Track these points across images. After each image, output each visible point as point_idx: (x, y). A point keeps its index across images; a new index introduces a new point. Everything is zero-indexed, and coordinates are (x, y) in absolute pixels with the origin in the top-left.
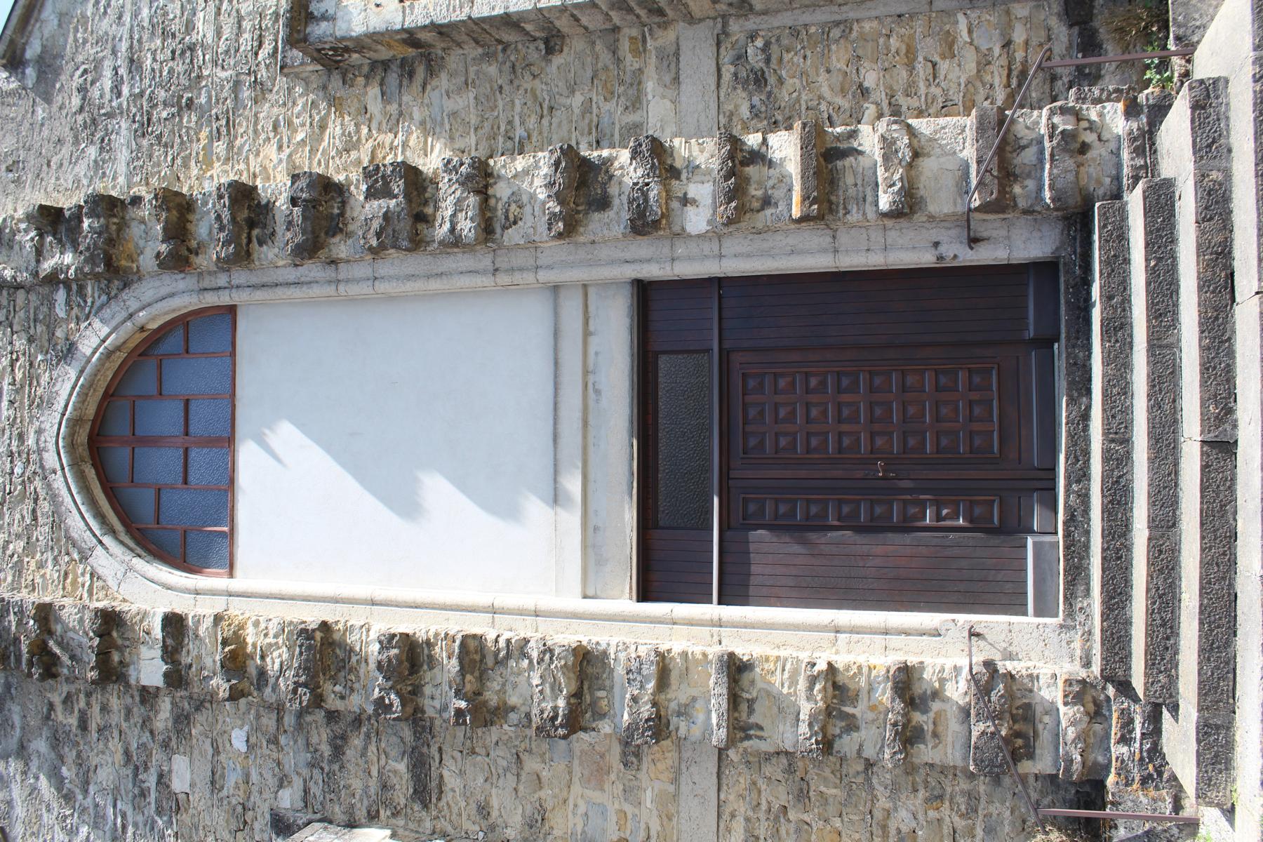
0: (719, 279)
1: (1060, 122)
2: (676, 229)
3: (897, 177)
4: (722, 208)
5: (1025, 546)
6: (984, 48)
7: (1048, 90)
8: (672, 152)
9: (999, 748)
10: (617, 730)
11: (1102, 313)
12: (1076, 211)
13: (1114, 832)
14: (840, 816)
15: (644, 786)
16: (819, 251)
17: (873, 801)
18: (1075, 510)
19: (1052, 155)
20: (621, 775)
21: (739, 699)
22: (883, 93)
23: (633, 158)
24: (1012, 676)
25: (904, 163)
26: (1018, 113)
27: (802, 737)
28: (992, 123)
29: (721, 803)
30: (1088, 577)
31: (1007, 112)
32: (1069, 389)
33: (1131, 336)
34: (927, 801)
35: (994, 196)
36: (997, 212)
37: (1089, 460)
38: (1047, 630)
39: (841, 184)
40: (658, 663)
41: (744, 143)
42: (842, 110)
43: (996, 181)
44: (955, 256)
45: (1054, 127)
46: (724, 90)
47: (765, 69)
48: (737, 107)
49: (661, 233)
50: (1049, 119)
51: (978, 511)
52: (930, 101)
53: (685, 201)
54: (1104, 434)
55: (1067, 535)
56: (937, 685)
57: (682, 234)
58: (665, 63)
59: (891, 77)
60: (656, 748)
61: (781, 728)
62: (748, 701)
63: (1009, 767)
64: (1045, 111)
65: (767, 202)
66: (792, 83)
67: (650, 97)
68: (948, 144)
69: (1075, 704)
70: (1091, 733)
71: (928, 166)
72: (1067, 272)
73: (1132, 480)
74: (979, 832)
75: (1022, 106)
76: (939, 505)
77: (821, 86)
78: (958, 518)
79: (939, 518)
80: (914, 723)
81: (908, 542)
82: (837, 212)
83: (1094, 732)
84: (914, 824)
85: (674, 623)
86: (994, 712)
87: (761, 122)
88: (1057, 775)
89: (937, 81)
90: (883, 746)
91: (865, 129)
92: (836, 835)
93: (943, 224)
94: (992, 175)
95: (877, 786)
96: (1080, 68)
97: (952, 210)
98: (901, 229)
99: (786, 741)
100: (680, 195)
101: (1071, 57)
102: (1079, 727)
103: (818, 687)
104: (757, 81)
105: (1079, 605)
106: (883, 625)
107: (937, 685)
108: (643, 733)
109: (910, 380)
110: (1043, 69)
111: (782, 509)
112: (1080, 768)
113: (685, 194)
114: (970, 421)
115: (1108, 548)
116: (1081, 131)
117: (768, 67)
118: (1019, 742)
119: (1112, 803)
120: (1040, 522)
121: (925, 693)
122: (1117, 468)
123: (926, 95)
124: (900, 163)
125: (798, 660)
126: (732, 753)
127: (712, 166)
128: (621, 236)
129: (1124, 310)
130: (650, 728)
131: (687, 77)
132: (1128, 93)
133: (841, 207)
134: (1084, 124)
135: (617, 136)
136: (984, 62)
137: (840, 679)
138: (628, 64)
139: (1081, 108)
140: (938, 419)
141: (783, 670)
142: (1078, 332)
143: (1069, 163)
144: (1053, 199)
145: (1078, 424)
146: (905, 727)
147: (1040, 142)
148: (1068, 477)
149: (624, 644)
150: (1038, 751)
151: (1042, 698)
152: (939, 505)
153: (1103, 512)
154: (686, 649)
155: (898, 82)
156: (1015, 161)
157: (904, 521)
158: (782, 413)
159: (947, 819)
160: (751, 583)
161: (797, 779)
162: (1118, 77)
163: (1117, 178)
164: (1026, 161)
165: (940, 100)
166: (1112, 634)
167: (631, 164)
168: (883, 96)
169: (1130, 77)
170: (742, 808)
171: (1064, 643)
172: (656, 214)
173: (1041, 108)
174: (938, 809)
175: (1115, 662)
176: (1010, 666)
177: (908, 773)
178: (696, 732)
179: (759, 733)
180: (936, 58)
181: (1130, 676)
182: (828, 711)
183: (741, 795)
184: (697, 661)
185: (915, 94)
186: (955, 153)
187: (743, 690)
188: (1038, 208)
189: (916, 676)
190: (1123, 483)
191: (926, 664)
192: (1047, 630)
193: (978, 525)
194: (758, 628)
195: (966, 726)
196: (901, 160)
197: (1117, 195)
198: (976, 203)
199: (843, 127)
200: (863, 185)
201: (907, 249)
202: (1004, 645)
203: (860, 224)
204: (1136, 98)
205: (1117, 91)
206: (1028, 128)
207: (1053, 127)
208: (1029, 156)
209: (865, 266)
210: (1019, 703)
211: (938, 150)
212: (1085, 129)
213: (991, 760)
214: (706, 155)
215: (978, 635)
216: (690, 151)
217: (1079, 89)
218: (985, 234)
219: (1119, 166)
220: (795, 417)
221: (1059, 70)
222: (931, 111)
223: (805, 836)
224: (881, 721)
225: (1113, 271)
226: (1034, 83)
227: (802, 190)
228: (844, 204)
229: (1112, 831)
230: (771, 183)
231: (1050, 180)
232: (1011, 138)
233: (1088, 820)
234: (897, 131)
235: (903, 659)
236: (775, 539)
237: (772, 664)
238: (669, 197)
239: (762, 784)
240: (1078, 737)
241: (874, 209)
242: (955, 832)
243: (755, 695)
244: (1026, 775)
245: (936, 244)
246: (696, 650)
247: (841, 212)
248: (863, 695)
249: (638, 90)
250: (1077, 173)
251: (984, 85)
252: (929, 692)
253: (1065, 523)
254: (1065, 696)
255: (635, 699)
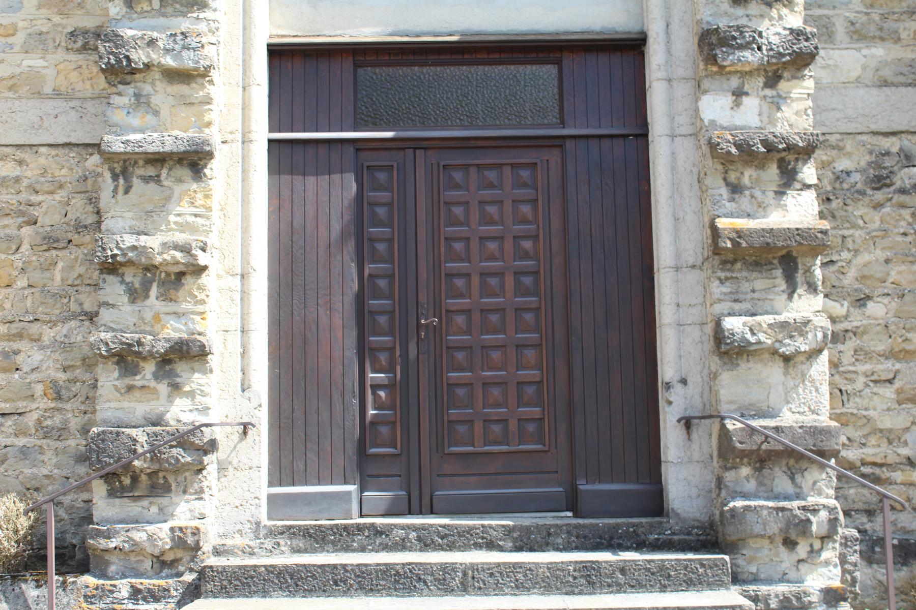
0: (645, 135)
1: (818, 523)
2: (706, 84)
3: (762, 337)
4: (730, 138)
5: (345, 483)
6: (908, 437)
7: (856, 507)
8: (797, 78)
9: (120, 459)
10: (114, 22)
11: (606, 562)
12: (720, 535)
13: (33, 584)
14: (30, 286)
15: (49, 57)
16: (677, 250)
17: (49, 322)
18: (387, 536)
19: (783, 509)
20: (60, 29)
21: (159, 164)
22: (859, 324)
23: (792, 31)
24: (200, 471)
25: (777, 345)
26: (833, 473)
27: (119, 239)
28: (820, 444)
29: (35, 149)
30: (314, 551)
31: (833, 460)
32: (521, 528)
33: (581, 593)
34: (54, 382)
35: (738, 445)
36: (720, 449)
37: (443, 550)
38: (253, 508)
39: (755, 274)
40: (196, 69)
41: (805, 162)
42: (841, 276)
43: (755, 447)
44: (670, 403)
45: (815, 511)
46: (870, 140)
47: (892, 188)
48: (849, 155)
49: (702, 66)
50: (824, 506)
51: (384, 430)
52: (849, 376)
53: (739, 94)
54: (472, 565)
55: (360, 528)
56: (187, 388)
57: (699, 89)
58: (905, 70)
59: (878, 333)
60: (95, 70)
61: (129, 215)
62: (158, 176)
63: (98, 470)
64: (833, 502)
65: (736, 189)
66: (875, 219)
67: (865, 52)
68: (798, 395)
69: (173, 539)
70: (141, 558)
71: (774, 372)
72: (651, 525)
73: (421, 595)
74: (22, 441)
75: (839, 478)
76: (389, 387)
77: (870, 252)
78: (375, 409)
79: (375, 387)
80: (142, 364)
81: (347, 353)
82: (722, 270)
83: (142, 561)
84: (26, 369)
85: (244, 88)
86: (160, 452)
87: (830, 183)
88: (92, 522)
89: (871, 384)
90: (113, 330)
91: (818, 301)
92: (6, 282)
93: (707, 389)
94: (762, 443)
95: (67, 326)
96: (881, 541)
97: (723, 398)
98: (702, 342)
99: (113, 221)
100: (746, 88)
101: (893, 532)
102: (146, 544)
103: (179, 255)
104: (879, 178)
105: (282, 542)
106: (252, 327)
107: (187, 388)
108: (112, 53)
109: (530, 354)
110: (881, 501)
111: (381, 211)
112: (101, 547)
113: (747, 94)
114: (485, 421)
115: (347, 571)
116: (810, 541)
117: (895, 192)
118: (127, 481)
119: (64, 582)
120: (371, 498)
121: (178, 376)
122: (435, 580)
123: (855, 372)
124: (777, 341)
125: (208, 232)
126: (95, 159)
127: (779, 125)
128: (698, 17)
129: (609, 586)
130: (119, 61)
131: (887, 95)
132: (851, 592)
133: (729, 274)
134: (817, 544)
135: (818, 12)
136: (891, 437)
137: (188, 280)
138: (907, 25)
139: (835, 541)
140: (487, 384)
141: (196, 216)
142: (585, 537)
143: (774, 527)
144: (733, 510)
145: (483, 538)
146: (138, 354)
147: (798, 497)
148: (423, 528)
149: (217, 29)
150: (117, 501)
151: (178, 504)
152: (389, 387)
153: (386, 565)
154: (214, 102)
155: (872, 340)
156: (777, 469)
157: (371, 349)
158: (492, 209)
159: (34, 406)
160: (295, 177)
161: (70, 236)
162: (869, 582)
163: (756, 580)
164: (777, 481)
165: (849, 388)
166: (252, 577)
167: (785, 29)
168: (856, 324)
169: (869, 596)
170: (30, 173)
171: (239, 527)
172: (724, 59)
173: (837, 498)
174: (45, 395)
175: (221, 580)
176: (211, 470)
177: (84, 360)
178: (118, 116)
179: (121, 190)
180: (898, 384)
181: (206, 597)
182: (150, 268)
183: (46, 171)
184: (200, 115)
185: (857, 360)
186: (788, 402)
187: (170, 169)
188: (723, 493)
189: (196, 365)
190: (420, 585)
191: (209, 375)
192: (253, 508)
193: (368, 430)
194: (243, 186)
195: (143, 422)
196: (780, 342)
197: (736, 579)
198: (730, 425)
199: (820, 277)
200: (753, 299)
201: (679, 349)
202: (235, 462)
203: (708, 295)
204: (845, 600)
205: (854, 581)
206: (815, 483)
207: (815, 510)
208: (782, 483)
209: (660, 302)
210: (171, 479)
211: (791, 384)
212: (811, 546)
213: (104, 450)
214: (793, 118)
215: (245, 433)
216: (797, 99)
217: (857, 540)
218: (695, 435)
219: (769, 581)
220: (486, 224)
221: (879, 519)
222: (837, 377)
223: (5, 245)
224: (143, 328)
225: (653, 574)
226: (865, 492)
227: (749, 230)
228: (732, 278)
229: (34, 583)
230: (758, 193)
231: (755, 507)
232: (804, 464)
233: (44, 558)
234: (813, 338)
235: (214, 350)
236: (346, 203)
237: (202, 202)
238: (743, 74)
239: (60, 196)
240: (136, 544)
241: (726, 312)
242: (20, 414)
243: (165, 183)
244: (90, 490)
245: (684, 382)
246: (214, 114)
247: (722, 275)
248: (172, 307)
249: (874, 37)
250: (762, 536)
251: (865, 436)
252: (178, 380)
253: (373, 525)
254: (181, 529)
255: (152, 43)
